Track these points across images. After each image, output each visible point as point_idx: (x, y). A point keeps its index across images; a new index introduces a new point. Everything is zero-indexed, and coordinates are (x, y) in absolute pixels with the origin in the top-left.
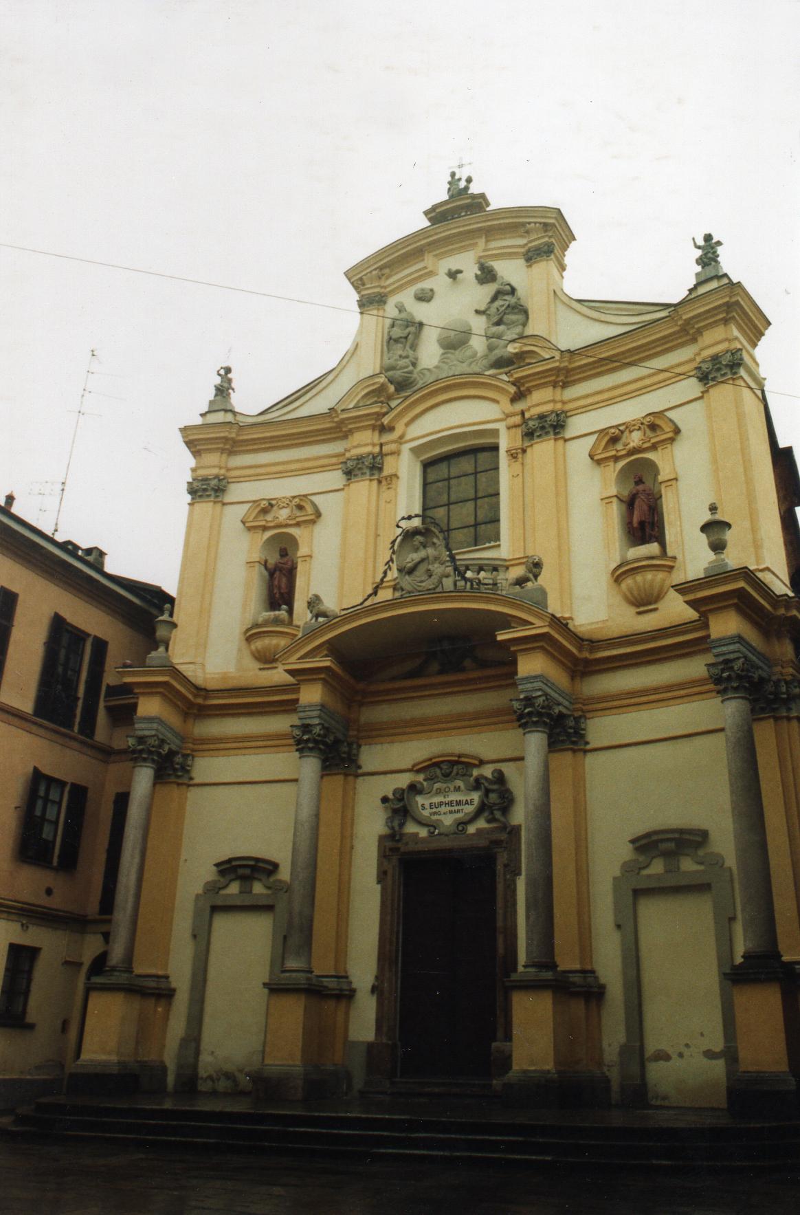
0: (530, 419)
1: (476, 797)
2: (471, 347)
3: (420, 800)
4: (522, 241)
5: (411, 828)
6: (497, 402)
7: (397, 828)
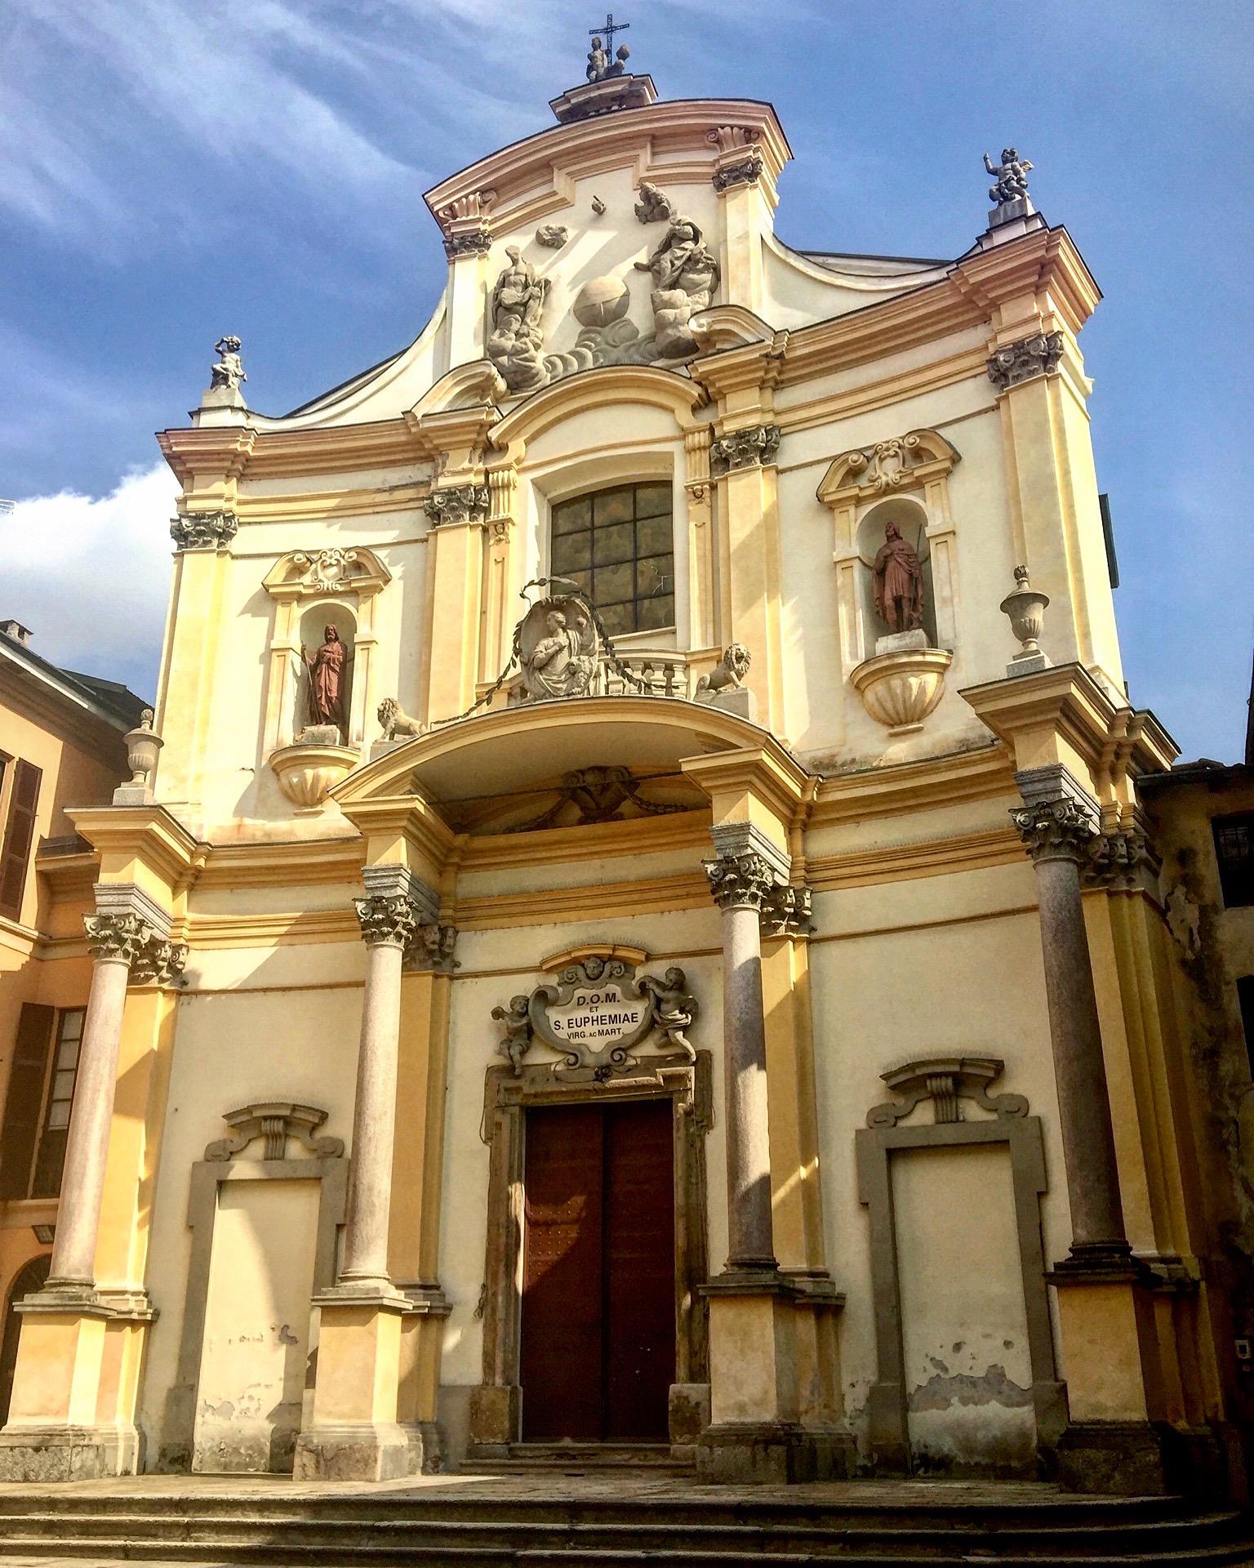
0: (724, 437)
1: (640, 1009)
2: (629, 322)
3: (553, 1015)
4: (710, 157)
5: (540, 1056)
6: (672, 411)
7: (517, 1057)
